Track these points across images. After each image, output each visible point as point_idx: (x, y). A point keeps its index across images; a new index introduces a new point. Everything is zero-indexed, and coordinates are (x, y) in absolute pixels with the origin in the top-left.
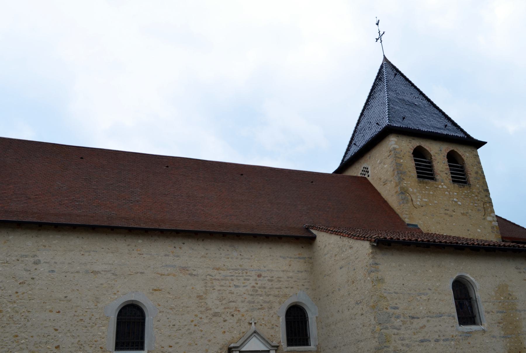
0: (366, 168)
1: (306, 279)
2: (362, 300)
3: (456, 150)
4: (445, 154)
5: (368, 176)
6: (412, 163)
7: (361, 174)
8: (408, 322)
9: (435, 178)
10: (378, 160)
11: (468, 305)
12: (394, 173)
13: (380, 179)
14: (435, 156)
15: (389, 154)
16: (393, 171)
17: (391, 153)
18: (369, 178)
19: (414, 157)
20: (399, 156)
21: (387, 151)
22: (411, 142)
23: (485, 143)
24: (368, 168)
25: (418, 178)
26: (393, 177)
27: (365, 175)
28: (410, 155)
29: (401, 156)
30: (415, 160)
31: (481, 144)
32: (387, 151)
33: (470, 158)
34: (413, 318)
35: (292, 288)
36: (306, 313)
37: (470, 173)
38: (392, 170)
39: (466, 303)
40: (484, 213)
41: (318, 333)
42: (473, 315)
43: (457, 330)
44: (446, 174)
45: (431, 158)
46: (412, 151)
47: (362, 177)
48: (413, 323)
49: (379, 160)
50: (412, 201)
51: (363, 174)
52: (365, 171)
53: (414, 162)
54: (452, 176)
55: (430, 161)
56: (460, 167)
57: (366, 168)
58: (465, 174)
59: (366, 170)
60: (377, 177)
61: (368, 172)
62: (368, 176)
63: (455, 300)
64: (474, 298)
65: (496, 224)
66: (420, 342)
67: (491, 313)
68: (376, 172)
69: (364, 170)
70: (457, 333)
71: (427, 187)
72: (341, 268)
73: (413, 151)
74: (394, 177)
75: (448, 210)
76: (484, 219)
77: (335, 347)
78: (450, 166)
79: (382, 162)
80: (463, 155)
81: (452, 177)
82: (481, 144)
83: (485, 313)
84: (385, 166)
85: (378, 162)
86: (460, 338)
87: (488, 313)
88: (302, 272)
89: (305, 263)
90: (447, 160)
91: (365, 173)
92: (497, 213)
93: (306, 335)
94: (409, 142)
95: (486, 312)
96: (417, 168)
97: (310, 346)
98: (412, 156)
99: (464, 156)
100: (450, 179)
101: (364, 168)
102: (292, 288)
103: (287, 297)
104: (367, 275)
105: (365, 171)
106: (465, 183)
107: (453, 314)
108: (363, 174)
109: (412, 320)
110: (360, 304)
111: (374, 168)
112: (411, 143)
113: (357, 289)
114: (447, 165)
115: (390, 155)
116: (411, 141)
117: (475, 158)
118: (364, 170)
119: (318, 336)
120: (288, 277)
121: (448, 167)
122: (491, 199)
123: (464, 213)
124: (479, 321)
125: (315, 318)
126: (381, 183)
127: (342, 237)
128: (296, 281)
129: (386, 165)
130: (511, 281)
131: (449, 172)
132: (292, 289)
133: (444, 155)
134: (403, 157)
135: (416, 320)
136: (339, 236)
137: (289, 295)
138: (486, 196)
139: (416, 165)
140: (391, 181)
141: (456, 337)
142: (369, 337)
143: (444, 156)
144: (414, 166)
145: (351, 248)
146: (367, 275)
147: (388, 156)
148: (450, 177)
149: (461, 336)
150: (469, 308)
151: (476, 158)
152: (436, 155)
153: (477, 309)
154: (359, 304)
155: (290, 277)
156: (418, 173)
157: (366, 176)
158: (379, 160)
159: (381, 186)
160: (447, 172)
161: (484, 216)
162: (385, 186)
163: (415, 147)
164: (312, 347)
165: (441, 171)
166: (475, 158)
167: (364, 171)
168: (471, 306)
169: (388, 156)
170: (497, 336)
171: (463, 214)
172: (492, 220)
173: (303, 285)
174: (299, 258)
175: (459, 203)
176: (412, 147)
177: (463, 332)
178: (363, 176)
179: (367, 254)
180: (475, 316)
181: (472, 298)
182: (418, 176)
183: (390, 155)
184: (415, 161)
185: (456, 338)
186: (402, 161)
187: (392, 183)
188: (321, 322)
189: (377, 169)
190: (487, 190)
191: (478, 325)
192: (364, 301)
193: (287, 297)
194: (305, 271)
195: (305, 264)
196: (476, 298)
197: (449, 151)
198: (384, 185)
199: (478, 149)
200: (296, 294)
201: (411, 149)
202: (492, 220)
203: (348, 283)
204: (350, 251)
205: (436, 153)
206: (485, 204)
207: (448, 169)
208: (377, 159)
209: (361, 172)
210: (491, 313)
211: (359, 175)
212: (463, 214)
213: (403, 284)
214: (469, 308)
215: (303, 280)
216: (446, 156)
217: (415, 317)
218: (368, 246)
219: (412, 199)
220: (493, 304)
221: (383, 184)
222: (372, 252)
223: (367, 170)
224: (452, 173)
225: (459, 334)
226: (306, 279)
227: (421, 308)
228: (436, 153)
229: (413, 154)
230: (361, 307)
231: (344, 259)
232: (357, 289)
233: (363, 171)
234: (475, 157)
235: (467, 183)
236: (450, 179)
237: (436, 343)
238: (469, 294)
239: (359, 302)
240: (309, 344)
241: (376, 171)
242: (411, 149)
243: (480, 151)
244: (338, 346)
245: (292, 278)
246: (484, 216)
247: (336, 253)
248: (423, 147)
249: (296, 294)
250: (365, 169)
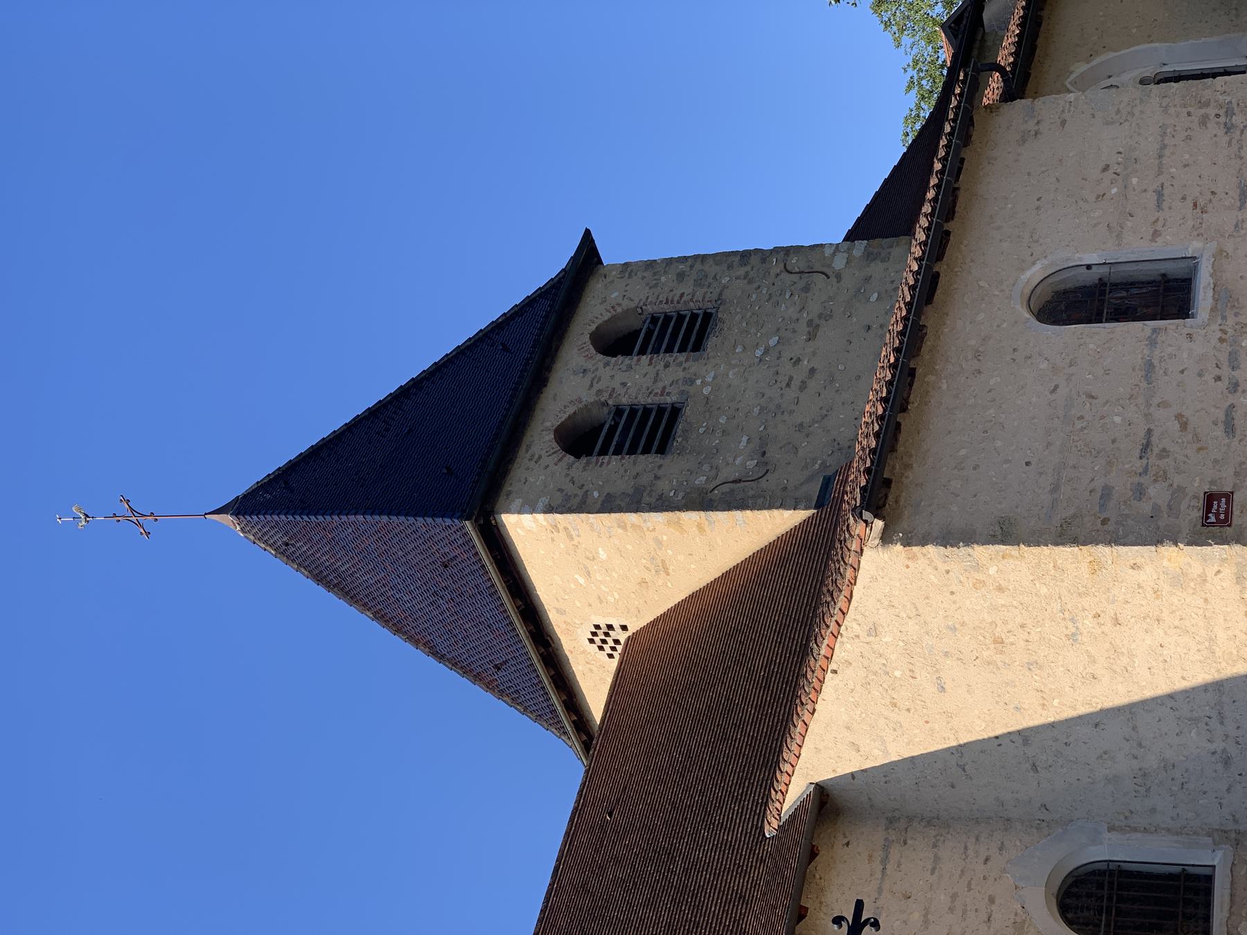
0: (594, 634)
1: (966, 848)
2: (1067, 613)
3: (593, 327)
4: (599, 361)
5: (624, 628)
6: (609, 463)
7: (611, 656)
8: (1162, 463)
9: (673, 404)
10: (576, 581)
11: (1124, 294)
12: (633, 525)
13: (643, 582)
14: (599, 392)
15: (563, 534)
16: (624, 528)
17: (561, 527)
18: (632, 629)
19: (589, 453)
20: (578, 499)
21: (553, 540)
22: (536, 456)
23: (587, 233)
24: (597, 627)
25: (666, 453)
26: (647, 533)
27: (617, 642)
28: (583, 465)
29: (580, 493)
30: (604, 452)
31: (587, 256)
32: (553, 540)
33: (628, 288)
34: (1146, 447)
35: (992, 900)
36: (1090, 868)
37: (678, 296)
38: (620, 531)
39: (1116, 298)
40: (820, 274)
41: (1168, 830)
42: (1160, 282)
43: (1204, 326)
44: (667, 366)
45: (605, 404)
46: (571, 458)
47: (622, 655)
48: (1164, 450)
49: (577, 576)
50: (740, 481)
51: (613, 649)
52: (603, 637)
53: (607, 457)
54: (680, 351)
55: (614, 409)
56: (652, 327)
57: (594, 634)
58: (659, 406)
59: (600, 635)
60: (633, 596)
61: (610, 627)
62: (624, 628)
63: (1101, 322)
64: (1105, 269)
65: (861, 245)
66: (1234, 436)
67: (1159, 226)
68: (617, 597)
69: (600, 644)
70: (1215, 327)
71: (701, 430)
72: (943, 689)
73: (568, 456)
74: (648, 529)
75: (791, 379)
76: (839, 277)
77: (1227, 761)
78: (642, 352)
79: (586, 568)
80: (613, 307)
81: (681, 350)
82: (587, 256)
83: (1156, 242)
84: (603, 555)
85: (582, 581)
86: (1231, 321)
87: (1156, 234)
88: (937, 859)
89: (905, 843)
90: (620, 358)
91: (609, 640)
92: (837, 235)
93: (1171, 876)
94: (536, 462)
95: (1153, 240)
96: (632, 451)
97: (1214, 867)
98: (584, 460)
99: (619, 305)
100: (687, 360)
101: (592, 641)
102: (992, 900)
103: (1024, 922)
104: (981, 577)
105: (603, 637)
106: (708, 316)
107: (1148, 332)
108: (613, 649)
109: (1156, 450)
110: (1080, 626)
111: (601, 602)
112: (540, 457)
113: (1022, 626)
114: (639, 360)
115: (566, 529)
116: (533, 456)
117: (630, 274)
118: (600, 644)
119: (1177, 834)
120: (951, 910)
121: (645, 357)
122: (776, 250)
123: (809, 333)
124: (1182, 264)
125: (1114, 836)
126: (660, 582)
127: (833, 666)
128: (969, 884)
129: (597, 553)
130: (1060, 160)
131: (662, 358)
132: (997, 901)
133: (601, 365)
134: (585, 489)
135: (1154, 439)
136: (829, 675)
137: (1016, 914)
138: (764, 261)
139: (617, 452)
140: (659, 542)
141: (1229, 330)
142: (1200, 602)
143: (607, 364)
144: (623, 458)
145: (874, 631)
146: (981, 577)
147: (571, 537)
148: (682, 357)
149: (1224, 318)
150: (1135, 291)
151: (632, 271)
152: (596, 387)
153: (1141, 266)
154: (1077, 628)
155: (953, 902)
156: (646, 451)
157: (623, 636)
158: (577, 576)
159: (669, 584)
160: (662, 363)
161: (828, 277)
162: (670, 571)
163: (557, 447)
164: (1215, 858)
165: (655, 381)
166: (633, 274)
167: (604, 641)
168: (1128, 285)
169: (571, 537)
170: (1237, 216)
171: (811, 337)
172: (846, 255)
173: (987, 860)
174: (885, 861)
175: (773, 341)
176: (555, 458)
177: (1212, 310)
178: (619, 648)
179: (909, 563)
180: (1164, 275)
181: (1100, 279)
182: (656, 453)
183: (566, 529)
184: (606, 454)
185: (1230, 331)
186: (596, 494)
187: (665, 538)
188: (1127, 814)
189: (607, 590)
190: (745, 256)
191: (1195, 269)
192: (1069, 606)
193: (1024, 922)
194: (935, 846)
195: (909, 842)
196: (1105, 264)
197: (591, 347)
198: (668, 574)
199: (600, 262)
200: (1016, 887)
201: (560, 460)
202: (846, 255)
203: (1000, 664)
204: (888, 639)
205: (591, 385)
206: (789, 268)
207: (651, 359)
208: (572, 586)
209: (602, 656)
210: (1159, 226)
211: (614, 663)
212: (811, 337)
213: (1028, 464)
214: (1135, 291)
215: (967, 857)
216: (608, 358)
217: (1145, 441)
218: (881, 553)
219: (733, 482)
220: (1130, 218)
221: (663, 574)
222: (901, 545)
223: (604, 629)
224: (669, 350)
225: (1219, 321)
226: (966, 848)
227: (1117, 419)
228: (591, 385)
229: (578, 457)
230: (1089, 622)
231: (911, 671)
232: (1022, 626)
233: (601, 648)
234: (627, 275)
235: (709, 311)
236: (687, 360)
237: (1240, 389)
238: (1074, 718)
239: (1070, 624)
240: (1207, 871)
241: (613, 596)
242: (560, 460)
243: (610, 254)
244: (1224, 750)
245: (954, 897)
246: (828, 277)
247: (888, 701)
248: (562, 424)
249: (1016, 887)
250: (595, 638)
